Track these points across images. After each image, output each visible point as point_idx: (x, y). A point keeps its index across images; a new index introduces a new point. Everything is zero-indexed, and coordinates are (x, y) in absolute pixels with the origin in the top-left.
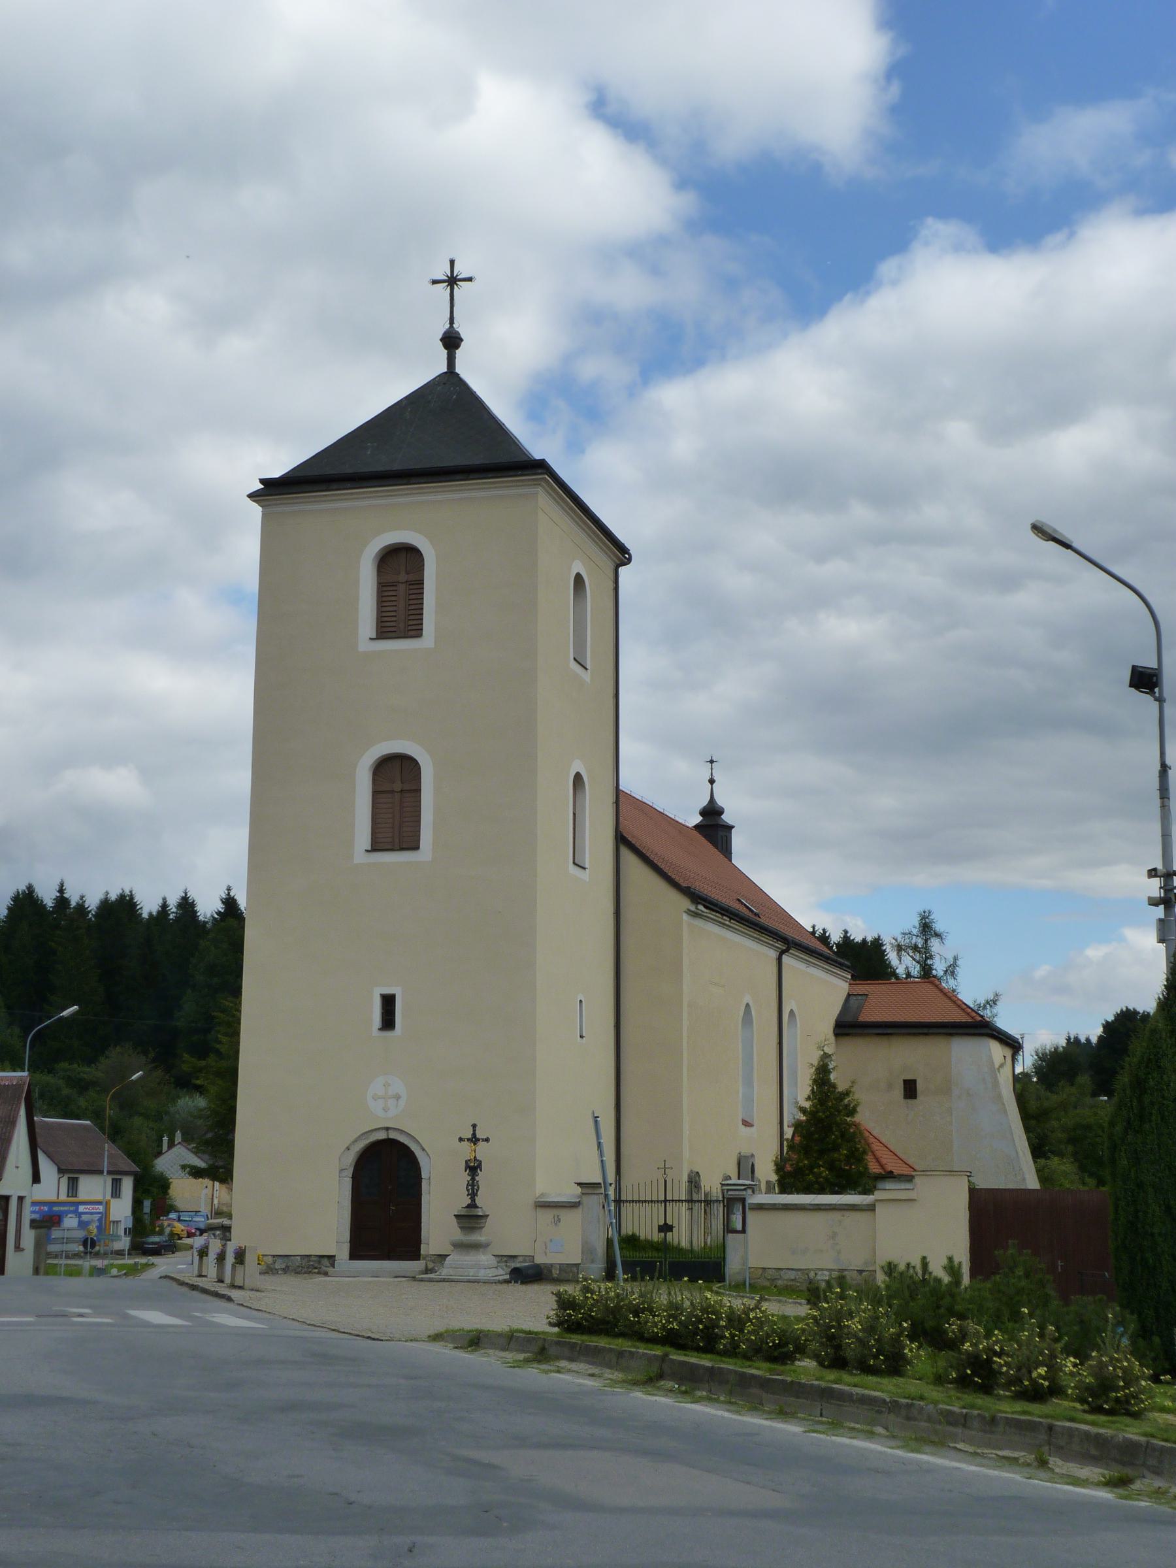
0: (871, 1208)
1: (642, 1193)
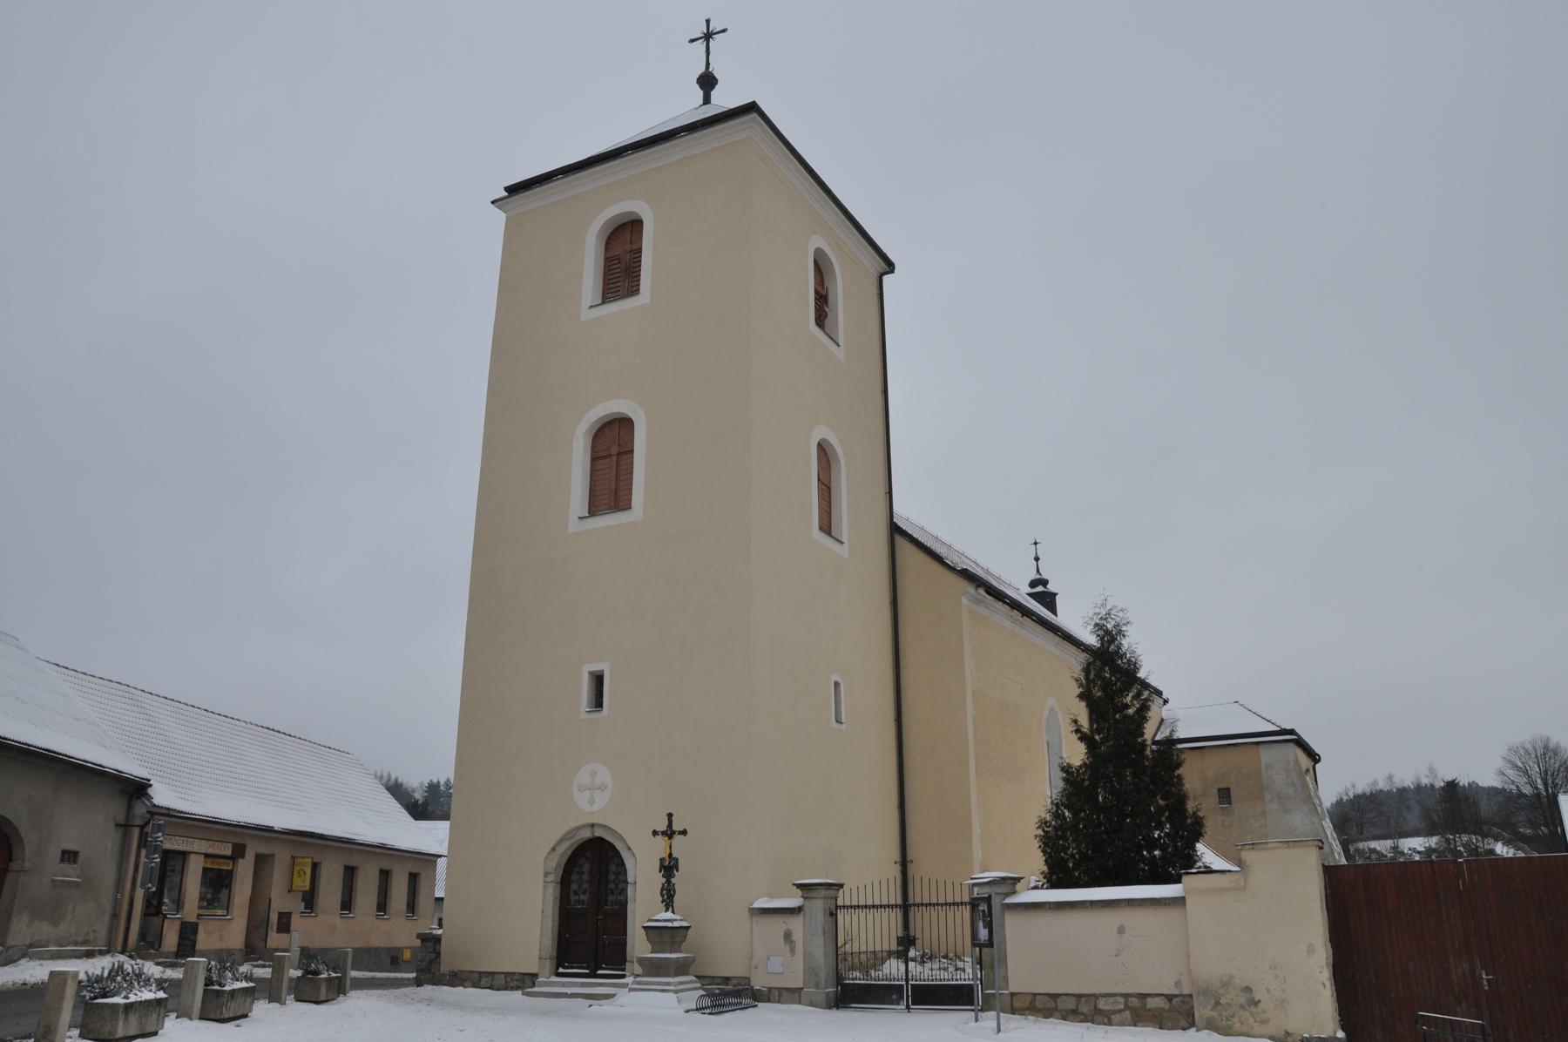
0: (1179, 902)
1: (926, 894)
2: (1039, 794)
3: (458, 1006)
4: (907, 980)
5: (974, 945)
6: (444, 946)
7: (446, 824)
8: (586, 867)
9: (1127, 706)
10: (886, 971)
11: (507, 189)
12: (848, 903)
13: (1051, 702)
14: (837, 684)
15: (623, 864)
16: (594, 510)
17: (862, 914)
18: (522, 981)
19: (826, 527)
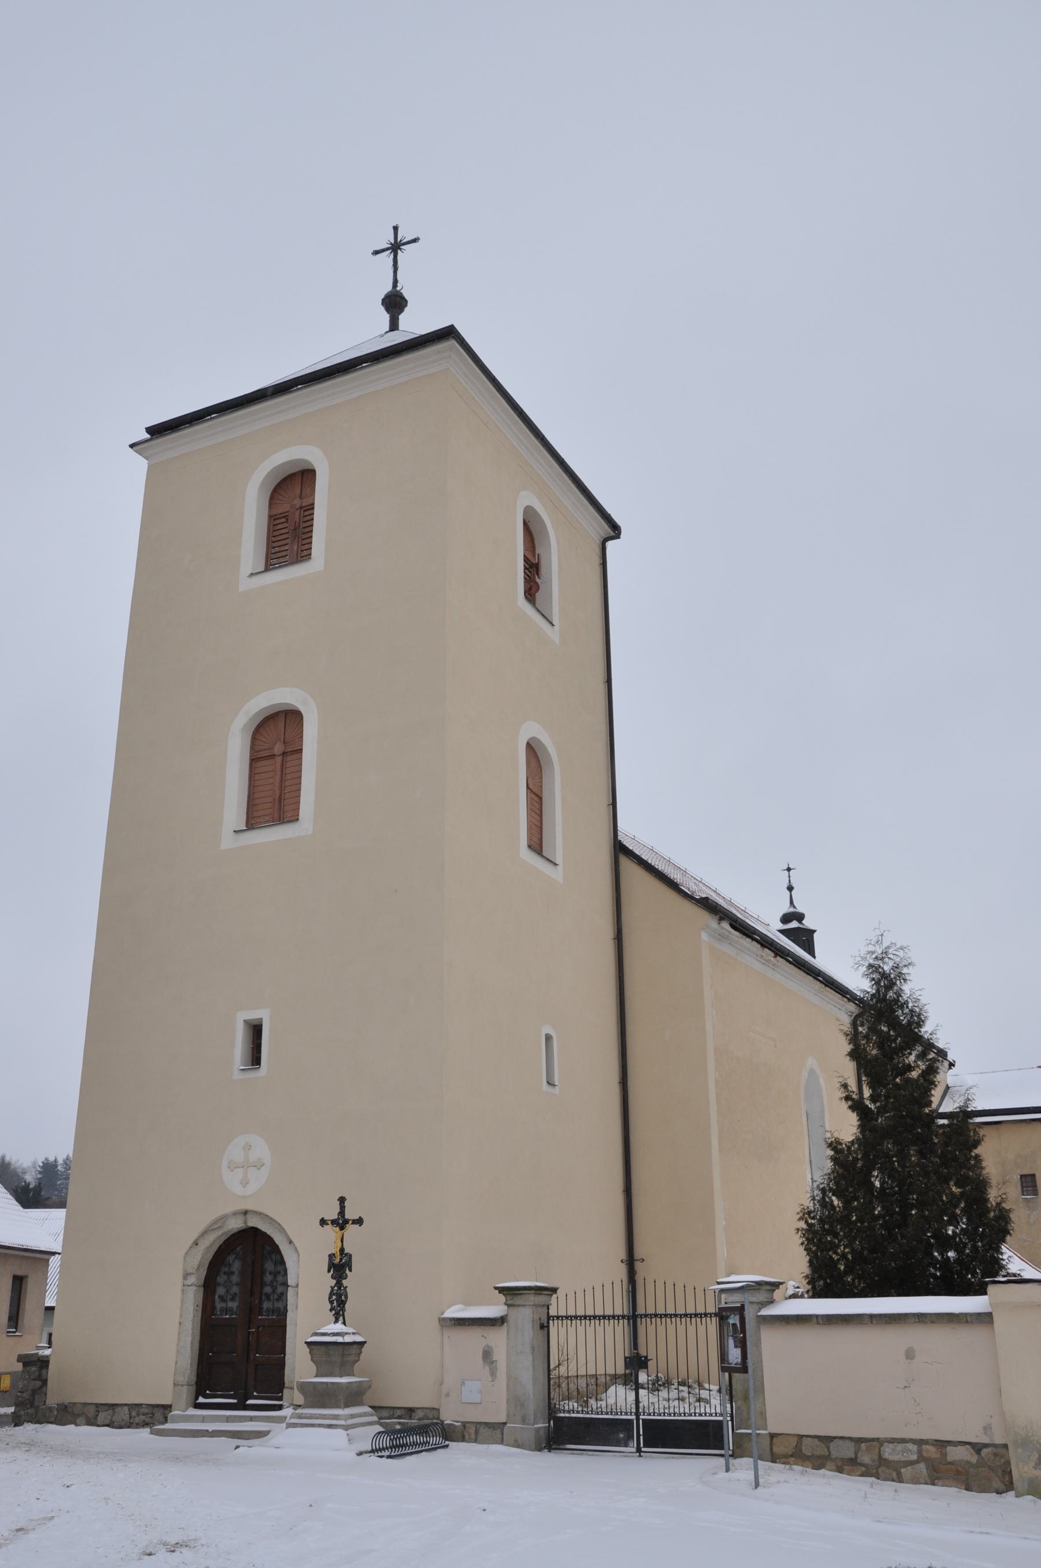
0: (985, 1319)
2: (799, 1180)
3: (66, 1451)
4: (637, 1414)
5: (724, 1369)
6: (52, 1371)
7: (60, 1214)
8: (237, 1266)
9: (909, 1068)
10: (611, 1401)
11: (149, 430)
12: (562, 1313)
13: (811, 1062)
14: (548, 1038)
15: (282, 1262)
16: (253, 821)
17: (580, 1326)
18: (151, 1416)
19: (537, 846)
